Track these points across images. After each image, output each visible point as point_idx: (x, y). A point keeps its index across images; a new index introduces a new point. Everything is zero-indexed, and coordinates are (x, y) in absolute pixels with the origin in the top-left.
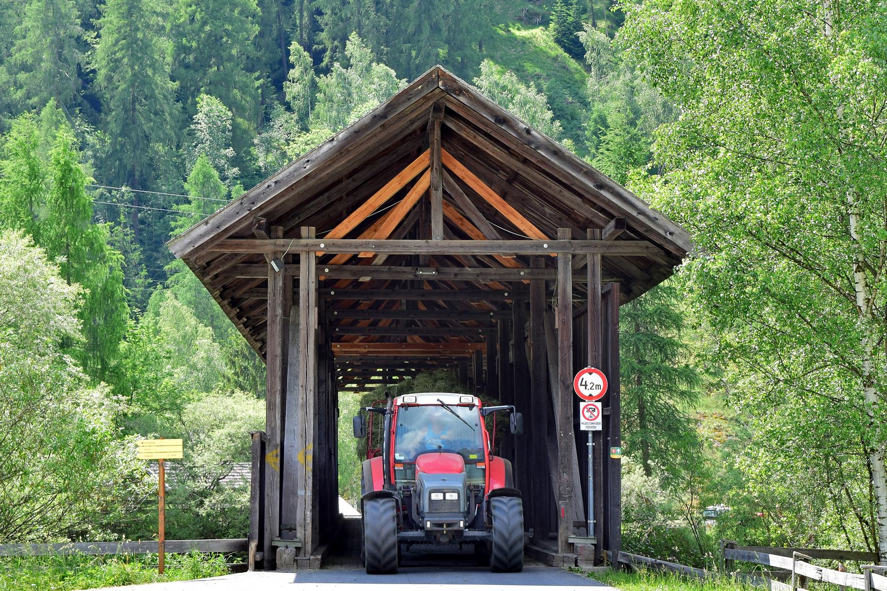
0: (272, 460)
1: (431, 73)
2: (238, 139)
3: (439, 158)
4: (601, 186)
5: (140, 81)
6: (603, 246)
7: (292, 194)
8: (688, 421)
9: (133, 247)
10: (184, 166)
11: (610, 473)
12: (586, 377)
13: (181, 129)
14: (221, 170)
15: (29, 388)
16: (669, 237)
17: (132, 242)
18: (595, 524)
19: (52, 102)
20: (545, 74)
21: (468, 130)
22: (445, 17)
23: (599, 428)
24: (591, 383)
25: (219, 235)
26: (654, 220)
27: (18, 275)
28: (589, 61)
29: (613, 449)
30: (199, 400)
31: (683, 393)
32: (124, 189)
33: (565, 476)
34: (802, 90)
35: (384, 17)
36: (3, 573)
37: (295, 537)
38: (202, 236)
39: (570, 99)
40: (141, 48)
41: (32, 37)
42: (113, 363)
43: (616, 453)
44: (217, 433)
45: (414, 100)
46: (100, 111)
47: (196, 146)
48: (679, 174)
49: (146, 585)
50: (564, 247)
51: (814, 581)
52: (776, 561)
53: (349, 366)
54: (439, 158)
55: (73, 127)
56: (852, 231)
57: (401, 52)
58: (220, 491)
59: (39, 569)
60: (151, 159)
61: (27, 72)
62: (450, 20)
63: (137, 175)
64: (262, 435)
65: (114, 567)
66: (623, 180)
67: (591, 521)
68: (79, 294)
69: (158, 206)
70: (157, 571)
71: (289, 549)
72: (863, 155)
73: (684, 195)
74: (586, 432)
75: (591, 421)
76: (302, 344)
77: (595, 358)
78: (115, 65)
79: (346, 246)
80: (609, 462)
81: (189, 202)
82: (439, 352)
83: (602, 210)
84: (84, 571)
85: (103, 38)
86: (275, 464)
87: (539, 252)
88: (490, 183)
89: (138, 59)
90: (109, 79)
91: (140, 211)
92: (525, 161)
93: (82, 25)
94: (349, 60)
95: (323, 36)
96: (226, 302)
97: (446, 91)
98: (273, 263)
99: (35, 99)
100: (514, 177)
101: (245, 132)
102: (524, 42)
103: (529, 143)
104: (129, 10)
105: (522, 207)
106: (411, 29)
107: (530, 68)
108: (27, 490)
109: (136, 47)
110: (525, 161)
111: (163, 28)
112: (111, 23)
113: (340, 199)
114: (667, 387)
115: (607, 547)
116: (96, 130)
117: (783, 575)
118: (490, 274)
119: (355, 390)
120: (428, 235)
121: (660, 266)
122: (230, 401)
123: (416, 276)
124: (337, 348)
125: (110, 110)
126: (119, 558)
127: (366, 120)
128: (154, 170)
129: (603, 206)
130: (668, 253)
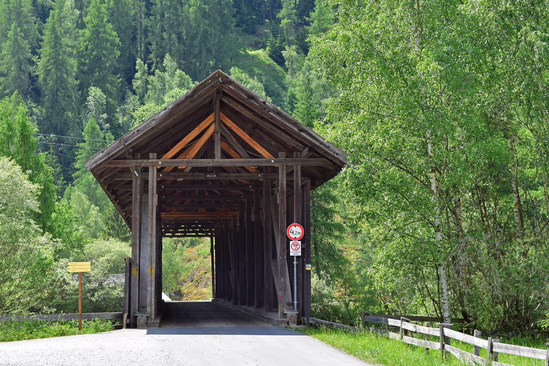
0: (135, 272)
1: (215, 74)
2: (109, 109)
3: (219, 117)
4: (302, 130)
5: (60, 81)
6: (301, 161)
7: (146, 136)
8: (339, 250)
9: (57, 165)
10: (82, 123)
11: (305, 277)
12: (293, 228)
13: (80, 104)
14: (100, 125)
15: (14, 237)
16: (336, 156)
17: (56, 163)
18: (297, 304)
19: (16, 92)
20: (264, 74)
21: (234, 103)
22: (214, 45)
23: (300, 254)
24: (296, 231)
25: (109, 158)
26: (328, 147)
27: (8, 180)
28: (287, 66)
29: (307, 265)
30: (92, 242)
31: (336, 237)
32: (52, 135)
33: (282, 279)
34: (403, 79)
35: (182, 46)
36: (2, 330)
37: (146, 311)
38: (100, 159)
39: (277, 86)
40: (61, 64)
41: (6, 59)
42: (49, 224)
43: (308, 267)
44: (101, 259)
45: (207, 88)
46: (40, 96)
47: (88, 113)
48: (340, 124)
49: (73, 336)
50: (281, 162)
51: (412, 332)
52: (392, 322)
53: (168, 224)
54: (219, 117)
55: (27, 104)
56: (429, 152)
57: (191, 63)
58: (103, 288)
59: (20, 328)
60: (66, 120)
61: (4, 77)
62: (216, 46)
63: (59, 128)
64: (130, 259)
65: (56, 327)
66: (311, 125)
67: (295, 302)
68: (38, 189)
69: (69, 144)
70: (77, 329)
71: (144, 318)
72: (435, 112)
73: (343, 134)
74: (293, 257)
75: (295, 251)
76: (150, 213)
77: (297, 218)
78: (47, 72)
79: (172, 162)
80: (305, 272)
81: (85, 142)
82: (214, 217)
83: (301, 142)
84: (42, 329)
85: (42, 59)
86: (136, 274)
87: (269, 165)
88: (243, 129)
89: (60, 69)
90: (45, 80)
91: (60, 146)
92: (262, 118)
93: (32, 53)
94: (165, 68)
95: (152, 56)
96: (109, 192)
97: (223, 83)
98: (135, 172)
99: (8, 91)
100: (256, 126)
101: (113, 105)
102: (254, 57)
103: (265, 109)
104: (55, 44)
105: (260, 141)
106: (196, 51)
107: (257, 71)
108: (12, 288)
109: (58, 64)
110: (262, 118)
111: (72, 53)
112: (46, 51)
113: (168, 139)
114: (329, 233)
115: (303, 316)
116: (38, 106)
117: (396, 329)
118: (243, 176)
119: (171, 237)
120: (213, 157)
121: (331, 171)
122: (107, 243)
123: (206, 178)
124: (163, 215)
125: (45, 95)
126: (59, 322)
127: (183, 99)
128: (67, 126)
129: (302, 140)
130: (335, 164)
